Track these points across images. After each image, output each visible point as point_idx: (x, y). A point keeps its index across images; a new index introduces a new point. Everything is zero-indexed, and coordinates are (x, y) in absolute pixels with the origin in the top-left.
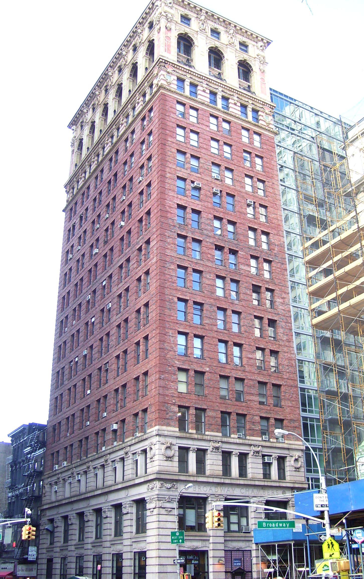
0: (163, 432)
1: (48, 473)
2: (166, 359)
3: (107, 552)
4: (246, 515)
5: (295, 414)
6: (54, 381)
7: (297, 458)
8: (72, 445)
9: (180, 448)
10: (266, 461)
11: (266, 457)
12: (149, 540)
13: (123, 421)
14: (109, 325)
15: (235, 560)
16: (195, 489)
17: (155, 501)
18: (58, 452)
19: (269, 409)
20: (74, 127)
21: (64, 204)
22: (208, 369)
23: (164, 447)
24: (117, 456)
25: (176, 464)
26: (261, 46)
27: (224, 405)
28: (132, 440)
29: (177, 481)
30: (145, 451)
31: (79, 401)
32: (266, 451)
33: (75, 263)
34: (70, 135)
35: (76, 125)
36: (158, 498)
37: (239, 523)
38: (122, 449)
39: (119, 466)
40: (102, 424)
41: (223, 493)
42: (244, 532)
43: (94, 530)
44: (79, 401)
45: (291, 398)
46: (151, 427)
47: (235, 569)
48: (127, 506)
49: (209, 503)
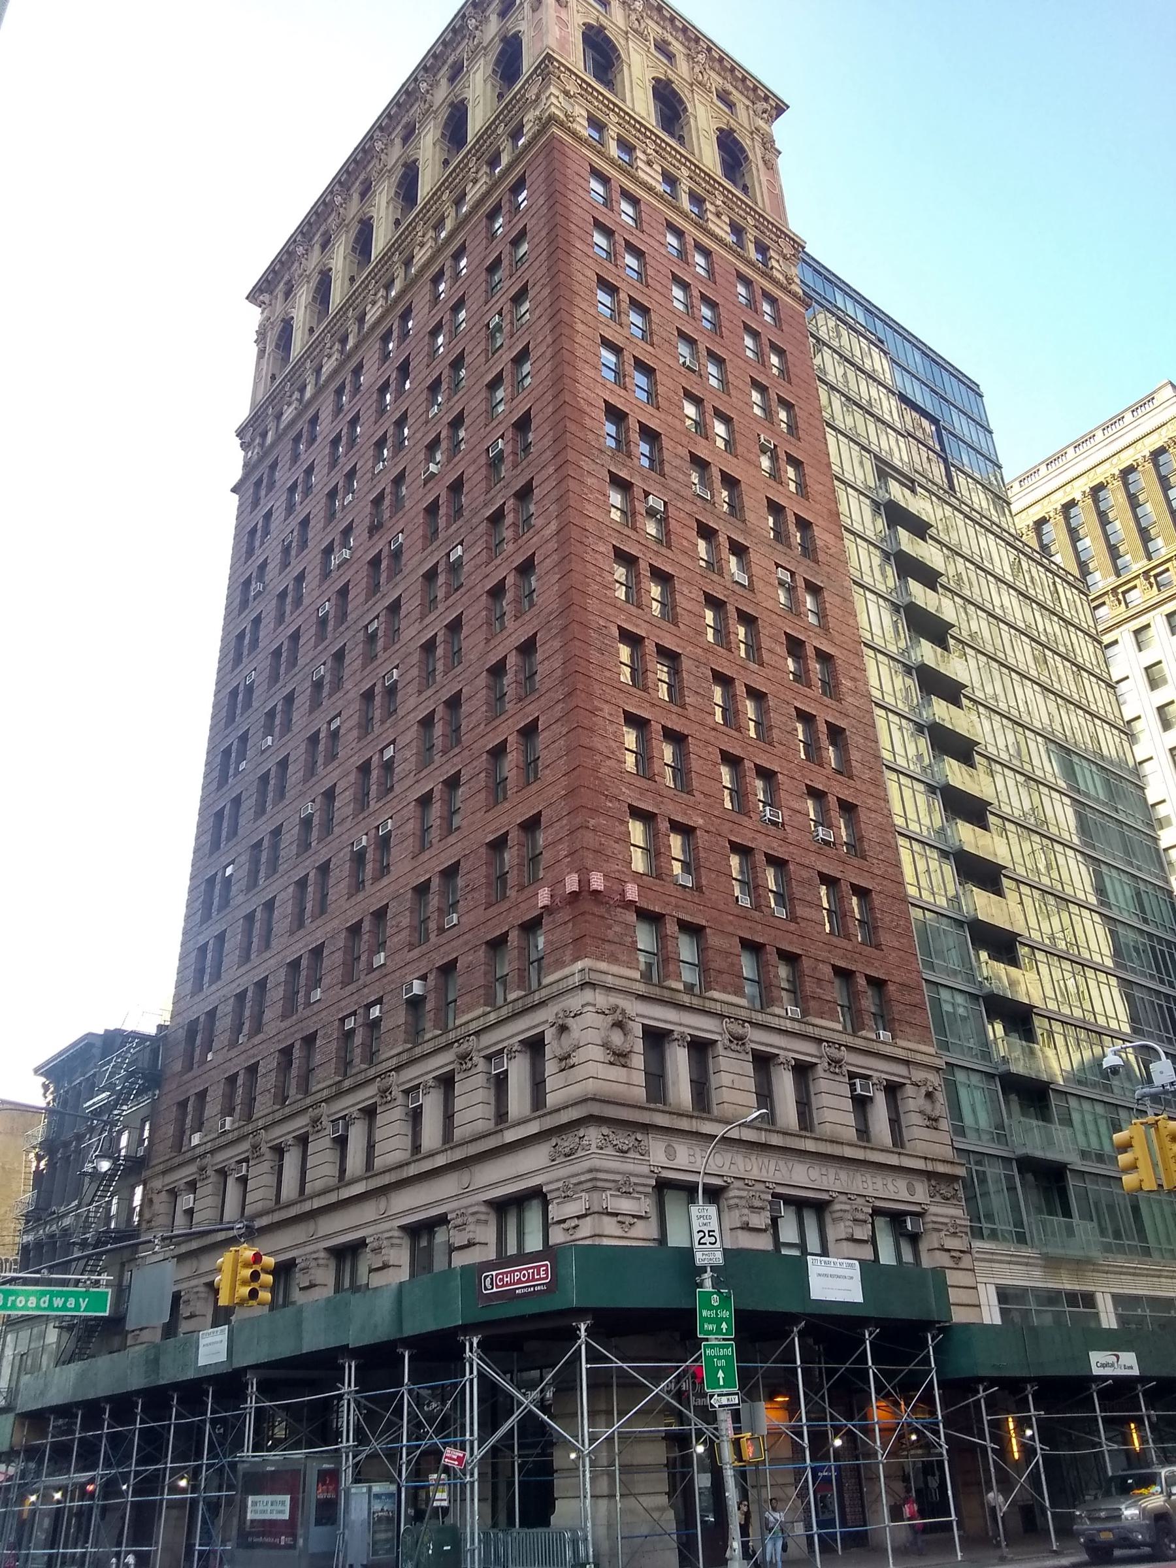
0: (603, 977)
2: (598, 778)
5: (909, 971)
6: (198, 904)
7: (931, 1089)
9: (647, 1030)
10: (859, 1091)
11: (857, 1081)
14: (394, 725)
20: (265, 297)
21: (237, 474)
22: (701, 821)
25: (640, 1078)
26: (765, 112)
27: (748, 924)
30: (535, 1046)
31: (284, 940)
33: (274, 602)
34: (253, 315)
35: (271, 293)
38: (449, 1045)
44: (284, 940)
45: (896, 927)
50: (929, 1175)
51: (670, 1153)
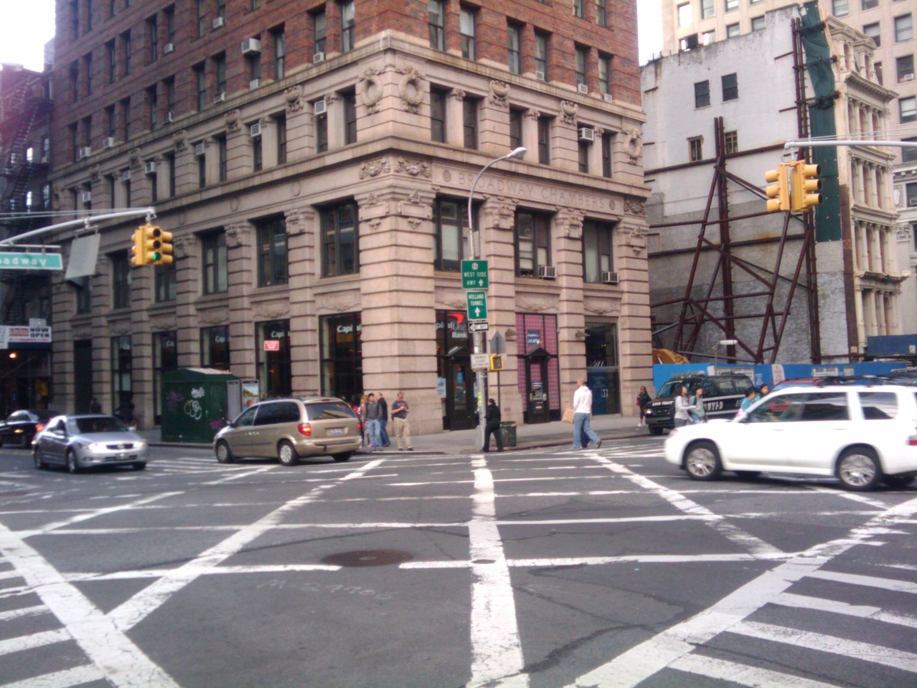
1: (64, 165)
3: (246, 315)
4: (545, 244)
7: (635, 137)
8: (126, 102)
12: (296, 296)
13: (277, 31)
15: (531, 332)
16: (462, 181)
17: (387, 200)
18: (88, 120)
19: (589, 28)
23: (403, 79)
24: (264, 112)
28: (308, 69)
29: (430, 159)
30: (348, 95)
32: (585, 116)
36: (394, 193)
37: (534, 260)
39: (212, 154)
40: (212, 45)
41: (512, 194)
42: (546, 279)
43: (199, 275)
46: (367, 32)
47: (530, 350)
48: (301, 216)
49: (486, 214)
50: (626, 197)
51: (447, 176)
